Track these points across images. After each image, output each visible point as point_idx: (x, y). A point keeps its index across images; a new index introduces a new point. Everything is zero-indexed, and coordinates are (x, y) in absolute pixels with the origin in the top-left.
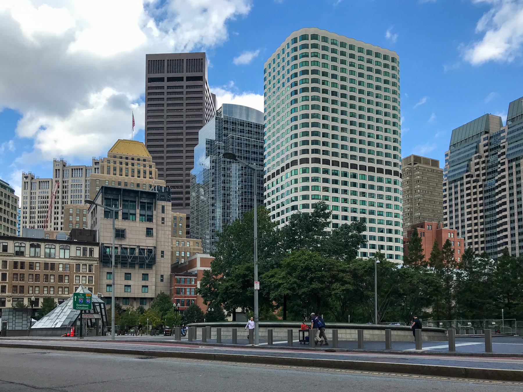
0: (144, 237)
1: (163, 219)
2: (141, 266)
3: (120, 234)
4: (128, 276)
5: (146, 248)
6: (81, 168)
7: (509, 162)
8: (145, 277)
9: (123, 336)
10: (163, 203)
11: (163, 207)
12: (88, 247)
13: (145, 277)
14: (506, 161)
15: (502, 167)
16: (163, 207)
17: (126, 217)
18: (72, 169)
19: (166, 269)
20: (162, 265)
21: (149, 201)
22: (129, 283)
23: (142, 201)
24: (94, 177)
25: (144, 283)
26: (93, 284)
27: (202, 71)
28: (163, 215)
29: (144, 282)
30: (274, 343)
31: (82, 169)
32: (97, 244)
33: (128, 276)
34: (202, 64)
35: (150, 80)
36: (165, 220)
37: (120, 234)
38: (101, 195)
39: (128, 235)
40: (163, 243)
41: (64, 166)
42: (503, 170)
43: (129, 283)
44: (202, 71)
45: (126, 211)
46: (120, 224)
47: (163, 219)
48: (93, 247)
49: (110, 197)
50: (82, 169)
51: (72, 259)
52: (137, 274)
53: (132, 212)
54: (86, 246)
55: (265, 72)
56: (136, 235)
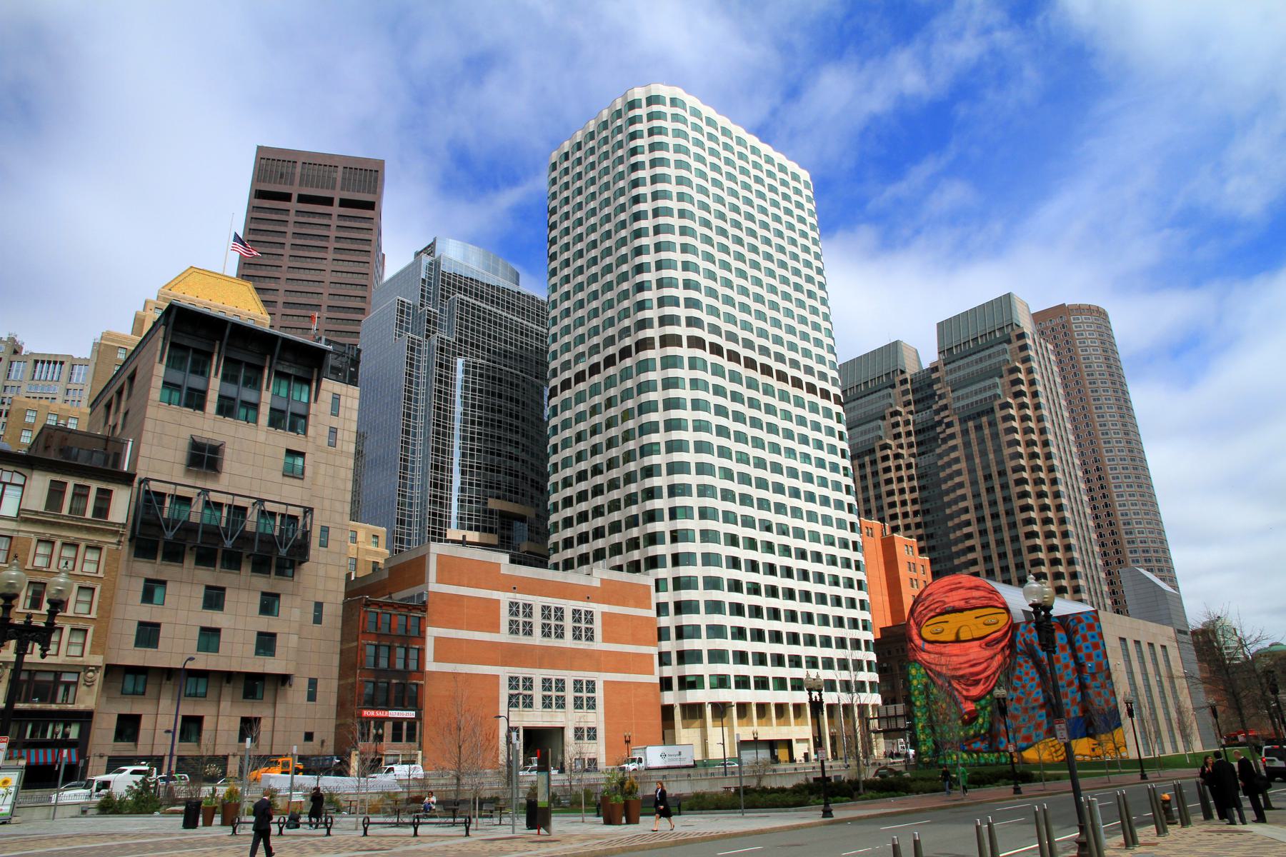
0: (278, 476)
1: (333, 431)
2: (261, 566)
3: (204, 458)
4: (214, 599)
5: (282, 509)
6: (59, 360)
7: (963, 421)
8: (269, 604)
9: (631, 828)
10: (338, 387)
11: (336, 398)
12: (94, 486)
13: (269, 604)
14: (955, 419)
15: (949, 431)
16: (336, 398)
17: (226, 407)
18: (36, 362)
19: (331, 585)
20: (321, 572)
21: (300, 374)
22: (214, 619)
23: (280, 368)
24: (113, 340)
25: (266, 623)
26: (93, 615)
27: (375, 192)
28: (335, 422)
29: (265, 618)
30: (183, 808)
31: (62, 363)
32: (127, 479)
33: (214, 599)
34: (376, 179)
35: (259, 194)
36: (339, 436)
37: (204, 458)
38: (161, 332)
39: (229, 463)
40: (327, 504)
41: (16, 352)
42: (952, 436)
43: (214, 619)
44: (375, 192)
45: (231, 390)
46: (208, 425)
47: (333, 431)
48: (110, 487)
49: (186, 342)
50: (62, 363)
51: (26, 521)
52: (243, 591)
53: (248, 395)
54: (87, 483)
55: (554, 167)
56: (254, 465)
